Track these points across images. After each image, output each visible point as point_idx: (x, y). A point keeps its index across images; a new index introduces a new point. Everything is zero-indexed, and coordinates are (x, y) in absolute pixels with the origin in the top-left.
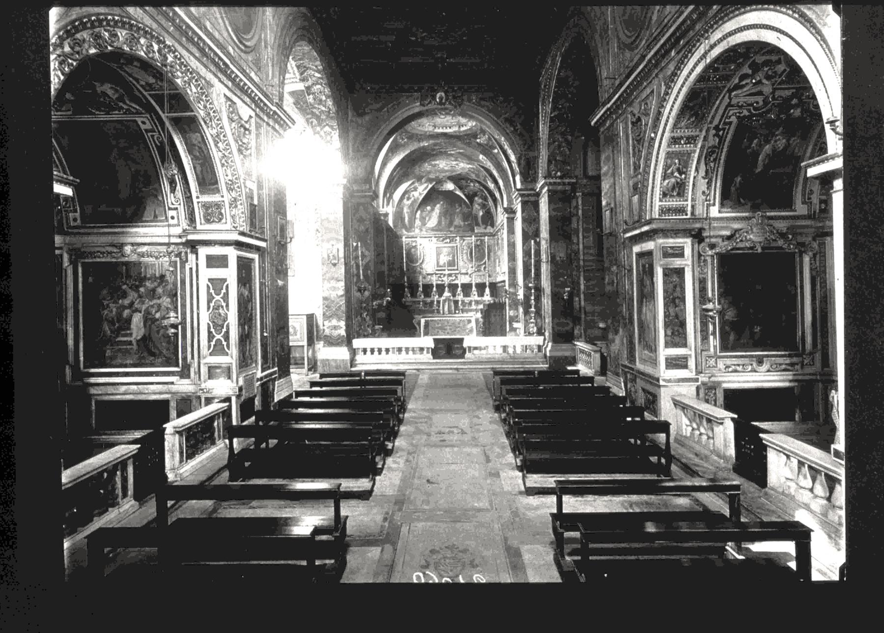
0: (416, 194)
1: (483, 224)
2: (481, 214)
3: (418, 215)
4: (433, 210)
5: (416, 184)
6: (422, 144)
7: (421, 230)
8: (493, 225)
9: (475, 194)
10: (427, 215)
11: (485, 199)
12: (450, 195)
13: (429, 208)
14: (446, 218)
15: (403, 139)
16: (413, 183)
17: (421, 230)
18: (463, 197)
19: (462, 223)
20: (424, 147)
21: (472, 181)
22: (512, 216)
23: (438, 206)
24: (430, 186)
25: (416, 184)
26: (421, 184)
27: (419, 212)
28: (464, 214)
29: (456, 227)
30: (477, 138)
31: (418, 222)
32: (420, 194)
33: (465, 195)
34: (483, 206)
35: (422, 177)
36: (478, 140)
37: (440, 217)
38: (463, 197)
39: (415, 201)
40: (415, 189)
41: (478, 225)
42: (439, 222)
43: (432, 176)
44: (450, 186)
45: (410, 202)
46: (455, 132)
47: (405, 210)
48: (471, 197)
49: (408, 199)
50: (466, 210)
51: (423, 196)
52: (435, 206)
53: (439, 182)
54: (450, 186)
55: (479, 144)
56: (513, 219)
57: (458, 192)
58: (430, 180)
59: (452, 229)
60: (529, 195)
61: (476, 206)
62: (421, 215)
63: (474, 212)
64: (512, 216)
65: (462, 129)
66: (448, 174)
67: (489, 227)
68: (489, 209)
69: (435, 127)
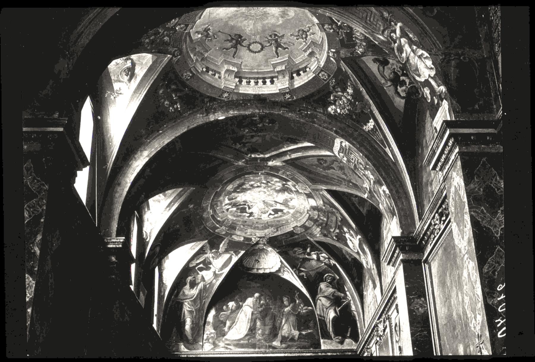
0: (208, 275)
1: (336, 334)
2: (332, 314)
3: (211, 317)
4: (239, 307)
5: (209, 255)
6: (212, 118)
7: (215, 345)
8: (355, 337)
9: (319, 277)
10: (228, 317)
11: (339, 285)
12: (273, 284)
13: (232, 304)
14: (264, 324)
15: (173, 103)
16: (201, 252)
17: (215, 345)
18: (298, 284)
19: (296, 333)
20: (217, 121)
21: (314, 248)
22: (415, 257)
23: (250, 301)
24: (235, 259)
25: (209, 255)
26: (218, 255)
27: (213, 312)
28: (299, 317)
29: (284, 339)
30: (326, 104)
31: (209, 330)
32: (216, 275)
33: (301, 278)
34: (336, 301)
35: (220, 238)
36: (331, 109)
37: (253, 321)
38: (298, 284)
39: (205, 289)
40: (207, 265)
41: (326, 336)
42: (252, 330)
43: (239, 237)
44: (271, 262)
45: (195, 292)
46: (282, 93)
47: (187, 307)
48: (312, 284)
49: (193, 285)
50: (303, 310)
51: (221, 279)
52: (244, 300)
53: (252, 250)
54: (271, 262)
55: (335, 117)
56: (418, 263)
57: (290, 276)
58: (234, 246)
59: (276, 343)
60: (480, 139)
61: (323, 301)
62: (216, 317)
63: (317, 312)
64: (415, 257)
65: (299, 82)
66: (269, 232)
67: (348, 341)
68: (348, 306)
69: (239, 76)
